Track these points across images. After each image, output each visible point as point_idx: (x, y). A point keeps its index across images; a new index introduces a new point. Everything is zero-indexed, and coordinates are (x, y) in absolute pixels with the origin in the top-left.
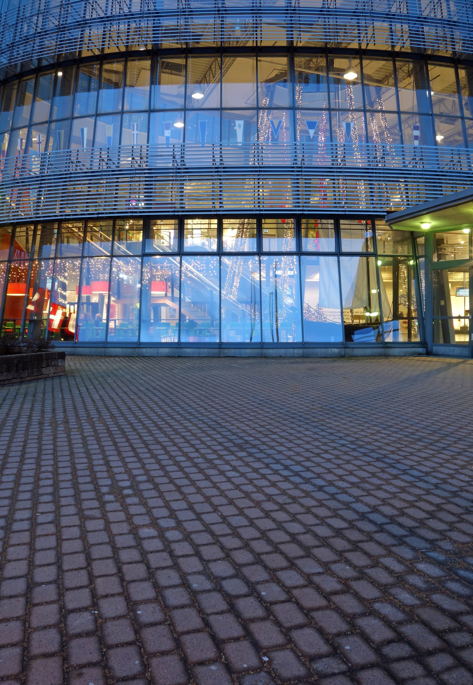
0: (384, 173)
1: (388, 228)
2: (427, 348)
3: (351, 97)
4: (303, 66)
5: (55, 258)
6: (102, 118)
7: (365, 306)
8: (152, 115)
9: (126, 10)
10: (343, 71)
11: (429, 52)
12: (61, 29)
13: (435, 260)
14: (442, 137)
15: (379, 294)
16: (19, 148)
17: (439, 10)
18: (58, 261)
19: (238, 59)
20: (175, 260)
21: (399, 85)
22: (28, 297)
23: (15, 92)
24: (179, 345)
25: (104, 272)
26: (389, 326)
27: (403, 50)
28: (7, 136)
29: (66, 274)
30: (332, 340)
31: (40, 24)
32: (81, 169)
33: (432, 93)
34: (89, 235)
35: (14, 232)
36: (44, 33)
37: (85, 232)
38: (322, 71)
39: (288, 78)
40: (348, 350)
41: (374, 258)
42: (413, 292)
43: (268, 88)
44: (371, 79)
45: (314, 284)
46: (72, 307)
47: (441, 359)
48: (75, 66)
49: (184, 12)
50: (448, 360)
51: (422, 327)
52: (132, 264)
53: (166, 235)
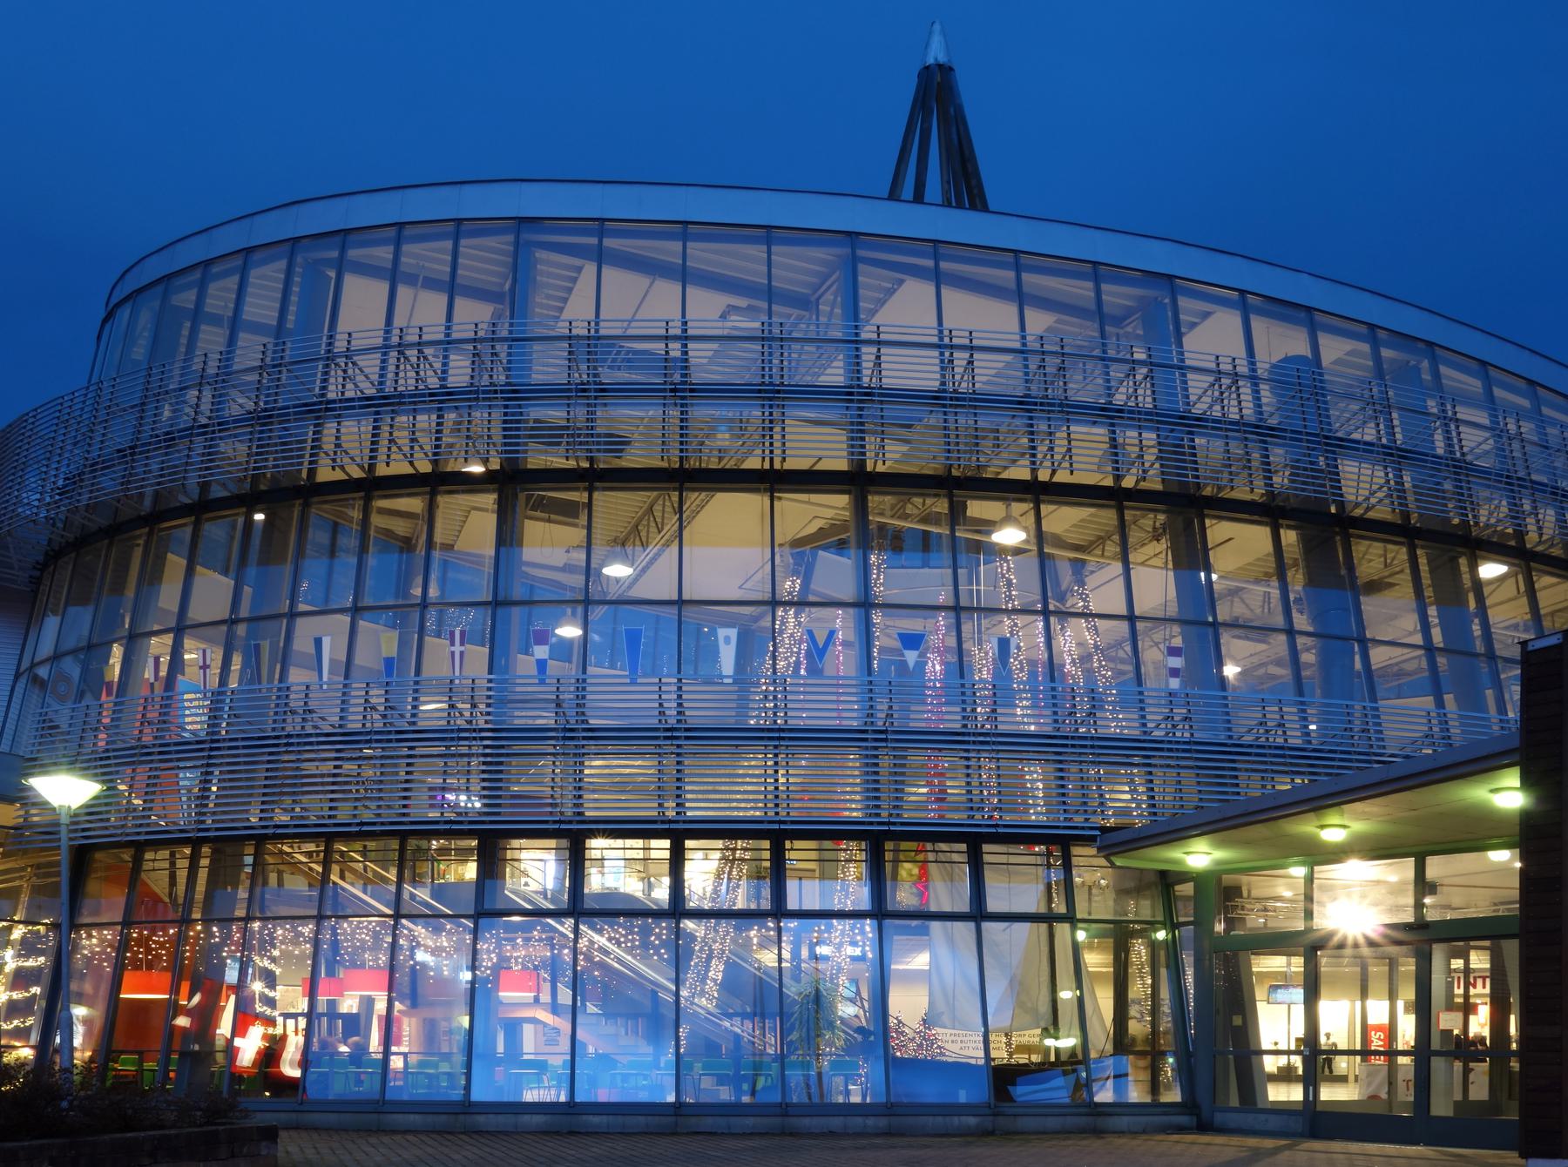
1: (1103, 862)
2: (1198, 1116)
3: (1010, 582)
4: (889, 513)
5: (248, 919)
6: (367, 614)
7: (1043, 1024)
8: (500, 611)
9: (433, 382)
10: (989, 525)
11: (1208, 491)
12: (261, 419)
13: (1220, 927)
14: (1238, 669)
15: (1081, 1001)
16: (148, 674)
17: (1234, 403)
18: (256, 925)
19: (719, 495)
20: (562, 924)
21: (1131, 557)
22: (176, 1001)
23: (138, 553)
25: (376, 948)
26: (1104, 1069)
27: (1143, 485)
28: (117, 651)
29: (276, 953)
30: (962, 1097)
31: (205, 407)
32: (316, 727)
33: (1214, 577)
34: (335, 868)
35: (138, 861)
36: (221, 426)
37: (326, 864)
38: (937, 523)
39: (850, 535)
40: (1001, 1120)
41: (1066, 926)
42: (1165, 993)
43: (798, 558)
44: (1059, 542)
45: (912, 977)
46: (291, 1023)
47: (1236, 1140)
49: (584, 390)
50: (1252, 1142)
51: (1186, 1073)
52: (449, 933)
53: (536, 869)
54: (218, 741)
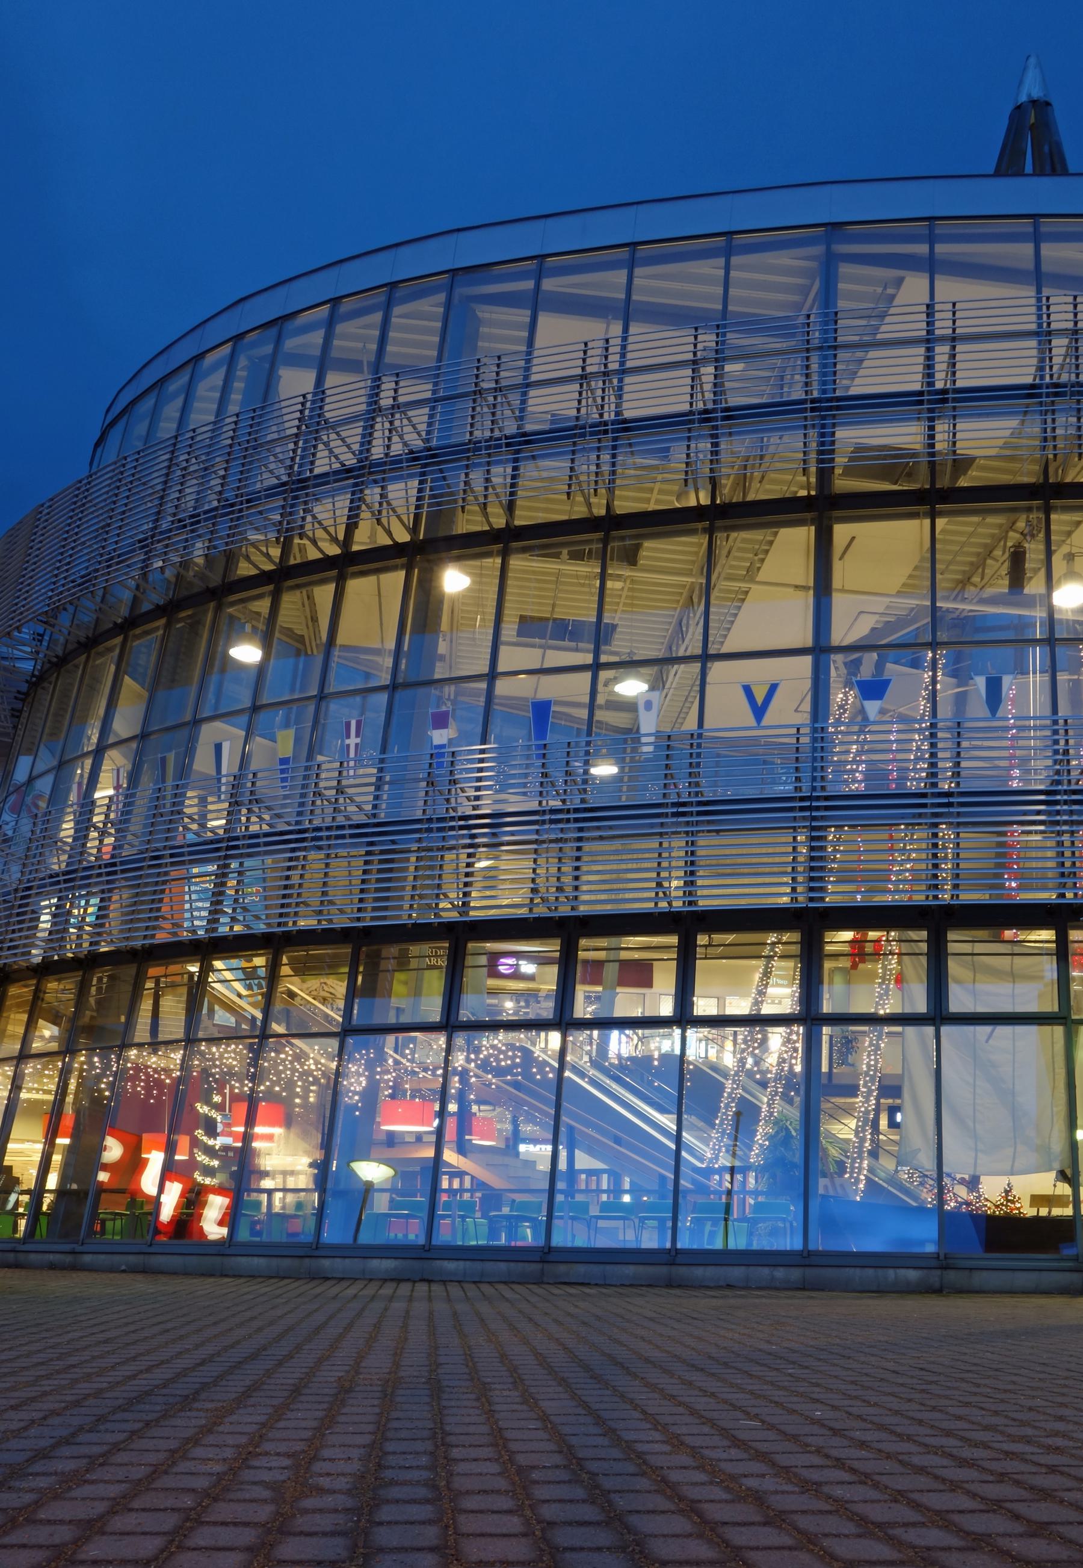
48: (212, 605)
54: (237, 838)
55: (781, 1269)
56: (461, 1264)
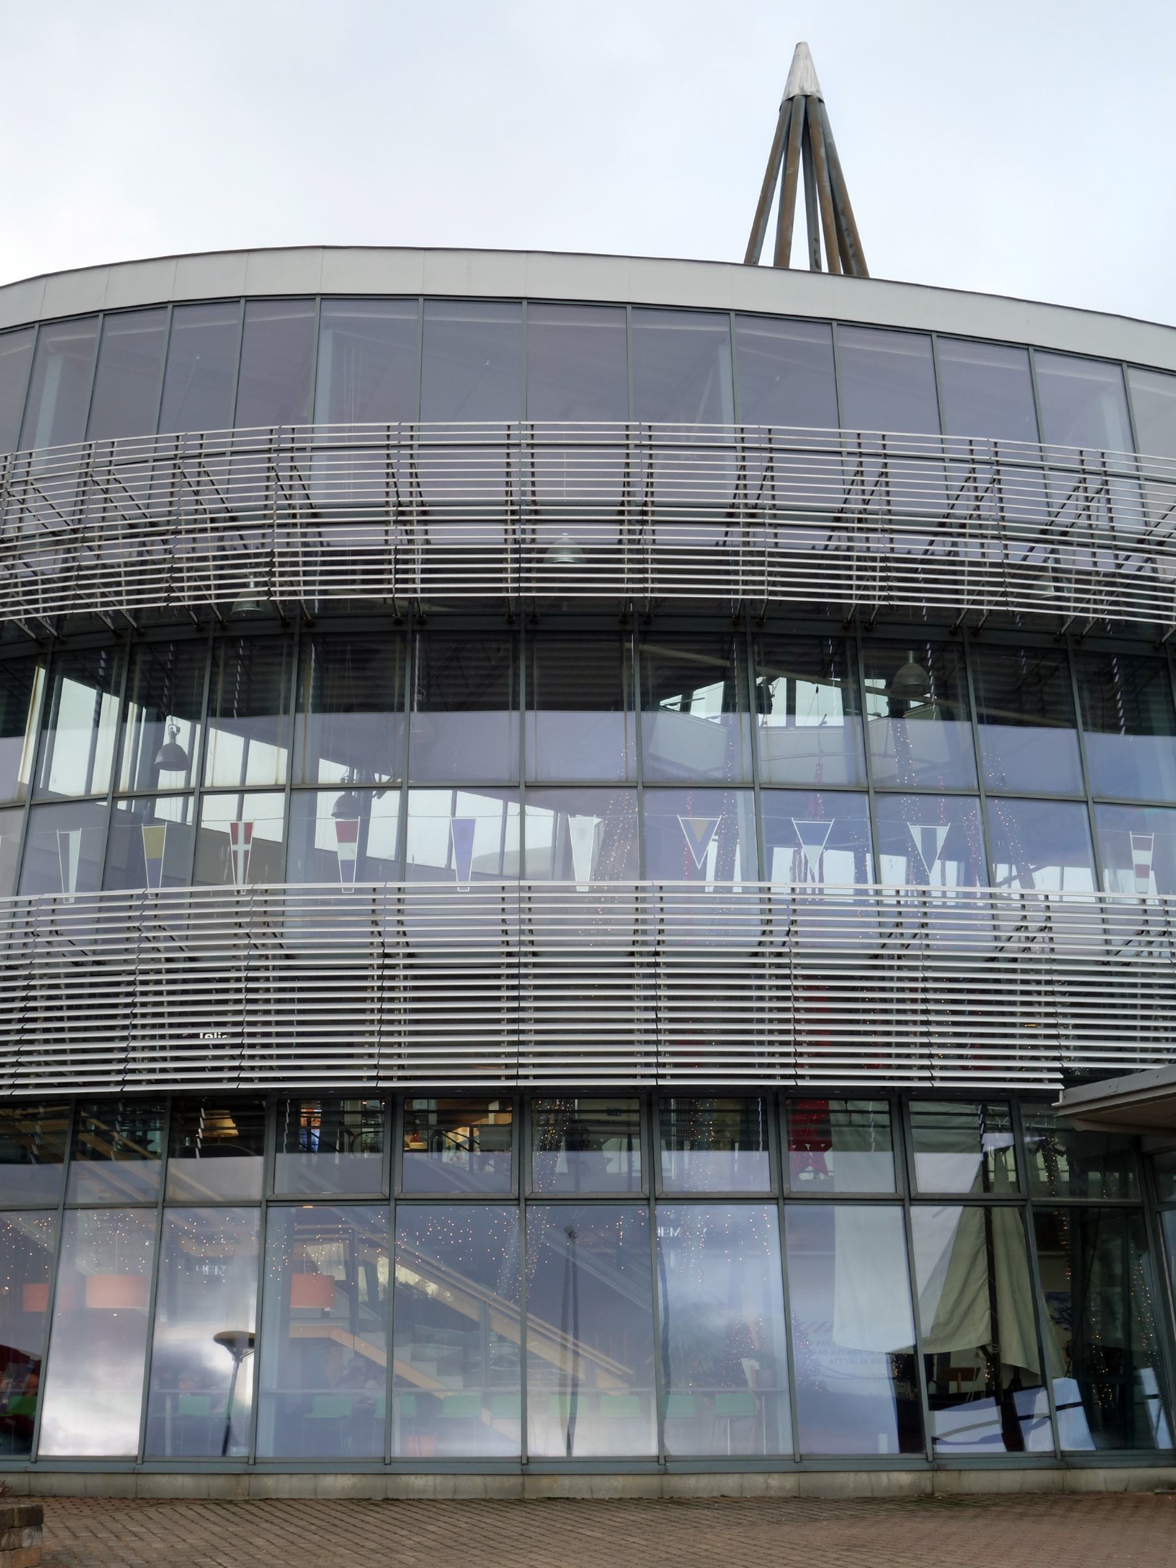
0: (1134, 996)
24: (663, 1464)
55: (776, 1476)
56: (431, 1478)
